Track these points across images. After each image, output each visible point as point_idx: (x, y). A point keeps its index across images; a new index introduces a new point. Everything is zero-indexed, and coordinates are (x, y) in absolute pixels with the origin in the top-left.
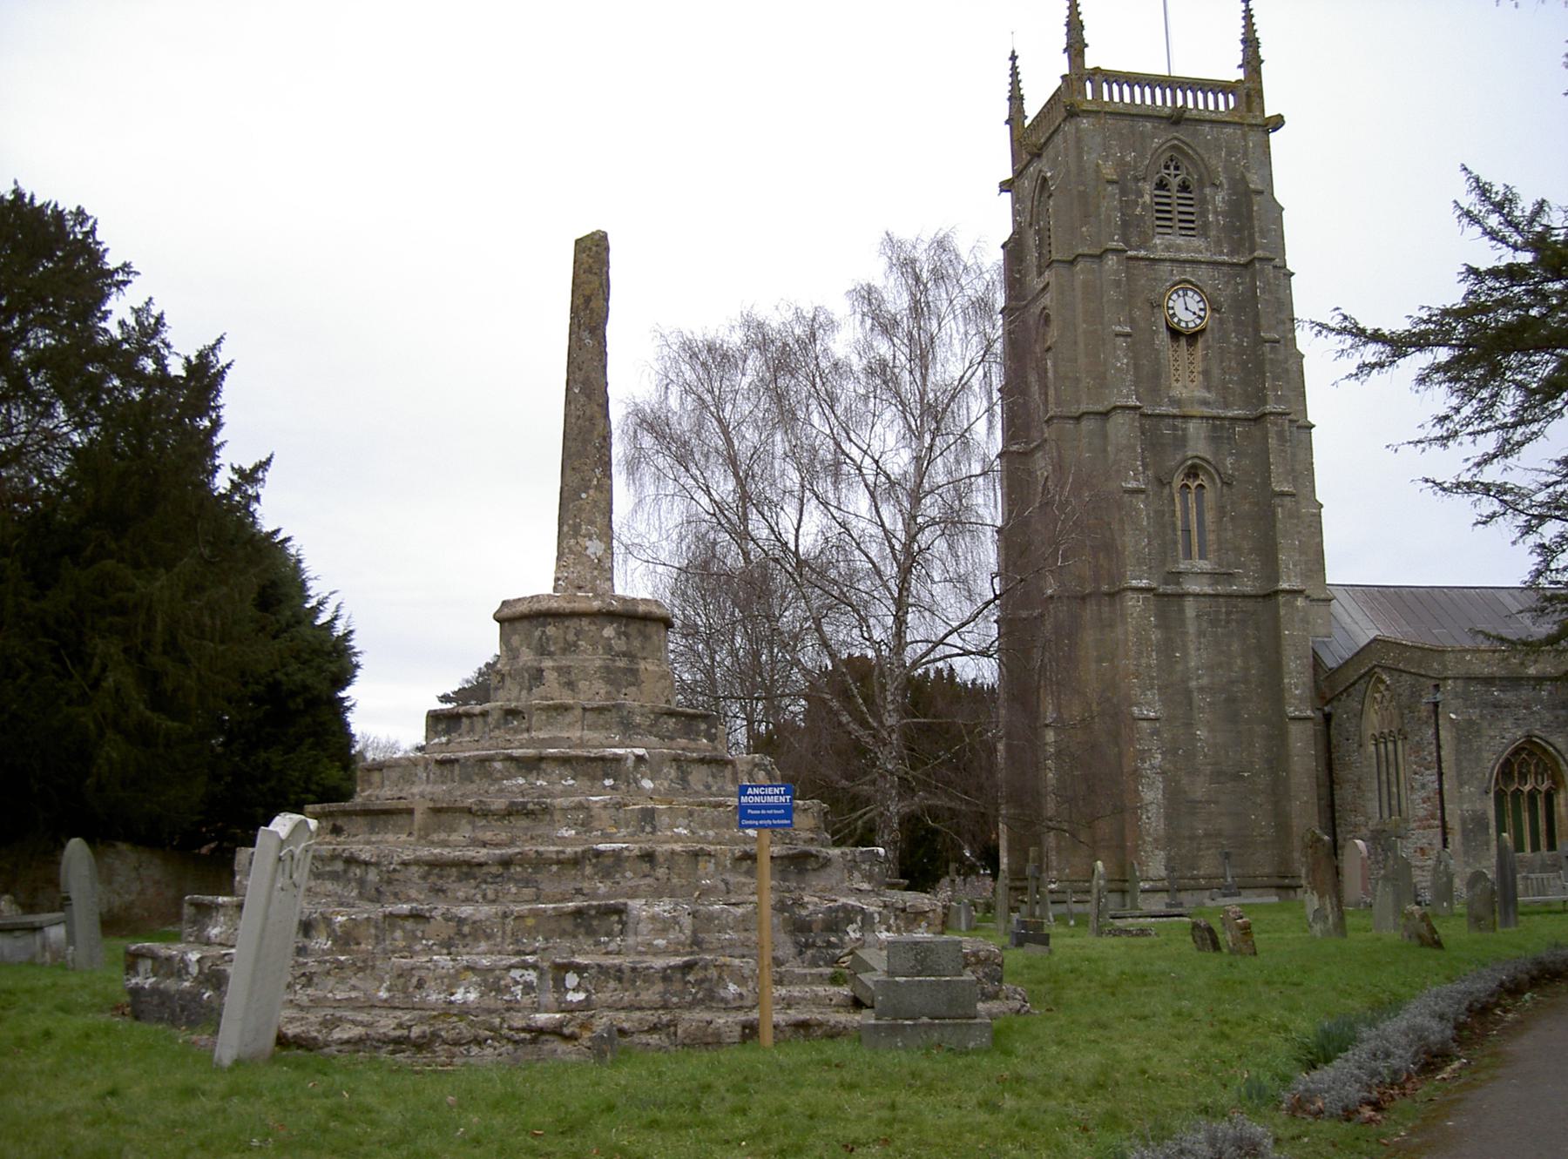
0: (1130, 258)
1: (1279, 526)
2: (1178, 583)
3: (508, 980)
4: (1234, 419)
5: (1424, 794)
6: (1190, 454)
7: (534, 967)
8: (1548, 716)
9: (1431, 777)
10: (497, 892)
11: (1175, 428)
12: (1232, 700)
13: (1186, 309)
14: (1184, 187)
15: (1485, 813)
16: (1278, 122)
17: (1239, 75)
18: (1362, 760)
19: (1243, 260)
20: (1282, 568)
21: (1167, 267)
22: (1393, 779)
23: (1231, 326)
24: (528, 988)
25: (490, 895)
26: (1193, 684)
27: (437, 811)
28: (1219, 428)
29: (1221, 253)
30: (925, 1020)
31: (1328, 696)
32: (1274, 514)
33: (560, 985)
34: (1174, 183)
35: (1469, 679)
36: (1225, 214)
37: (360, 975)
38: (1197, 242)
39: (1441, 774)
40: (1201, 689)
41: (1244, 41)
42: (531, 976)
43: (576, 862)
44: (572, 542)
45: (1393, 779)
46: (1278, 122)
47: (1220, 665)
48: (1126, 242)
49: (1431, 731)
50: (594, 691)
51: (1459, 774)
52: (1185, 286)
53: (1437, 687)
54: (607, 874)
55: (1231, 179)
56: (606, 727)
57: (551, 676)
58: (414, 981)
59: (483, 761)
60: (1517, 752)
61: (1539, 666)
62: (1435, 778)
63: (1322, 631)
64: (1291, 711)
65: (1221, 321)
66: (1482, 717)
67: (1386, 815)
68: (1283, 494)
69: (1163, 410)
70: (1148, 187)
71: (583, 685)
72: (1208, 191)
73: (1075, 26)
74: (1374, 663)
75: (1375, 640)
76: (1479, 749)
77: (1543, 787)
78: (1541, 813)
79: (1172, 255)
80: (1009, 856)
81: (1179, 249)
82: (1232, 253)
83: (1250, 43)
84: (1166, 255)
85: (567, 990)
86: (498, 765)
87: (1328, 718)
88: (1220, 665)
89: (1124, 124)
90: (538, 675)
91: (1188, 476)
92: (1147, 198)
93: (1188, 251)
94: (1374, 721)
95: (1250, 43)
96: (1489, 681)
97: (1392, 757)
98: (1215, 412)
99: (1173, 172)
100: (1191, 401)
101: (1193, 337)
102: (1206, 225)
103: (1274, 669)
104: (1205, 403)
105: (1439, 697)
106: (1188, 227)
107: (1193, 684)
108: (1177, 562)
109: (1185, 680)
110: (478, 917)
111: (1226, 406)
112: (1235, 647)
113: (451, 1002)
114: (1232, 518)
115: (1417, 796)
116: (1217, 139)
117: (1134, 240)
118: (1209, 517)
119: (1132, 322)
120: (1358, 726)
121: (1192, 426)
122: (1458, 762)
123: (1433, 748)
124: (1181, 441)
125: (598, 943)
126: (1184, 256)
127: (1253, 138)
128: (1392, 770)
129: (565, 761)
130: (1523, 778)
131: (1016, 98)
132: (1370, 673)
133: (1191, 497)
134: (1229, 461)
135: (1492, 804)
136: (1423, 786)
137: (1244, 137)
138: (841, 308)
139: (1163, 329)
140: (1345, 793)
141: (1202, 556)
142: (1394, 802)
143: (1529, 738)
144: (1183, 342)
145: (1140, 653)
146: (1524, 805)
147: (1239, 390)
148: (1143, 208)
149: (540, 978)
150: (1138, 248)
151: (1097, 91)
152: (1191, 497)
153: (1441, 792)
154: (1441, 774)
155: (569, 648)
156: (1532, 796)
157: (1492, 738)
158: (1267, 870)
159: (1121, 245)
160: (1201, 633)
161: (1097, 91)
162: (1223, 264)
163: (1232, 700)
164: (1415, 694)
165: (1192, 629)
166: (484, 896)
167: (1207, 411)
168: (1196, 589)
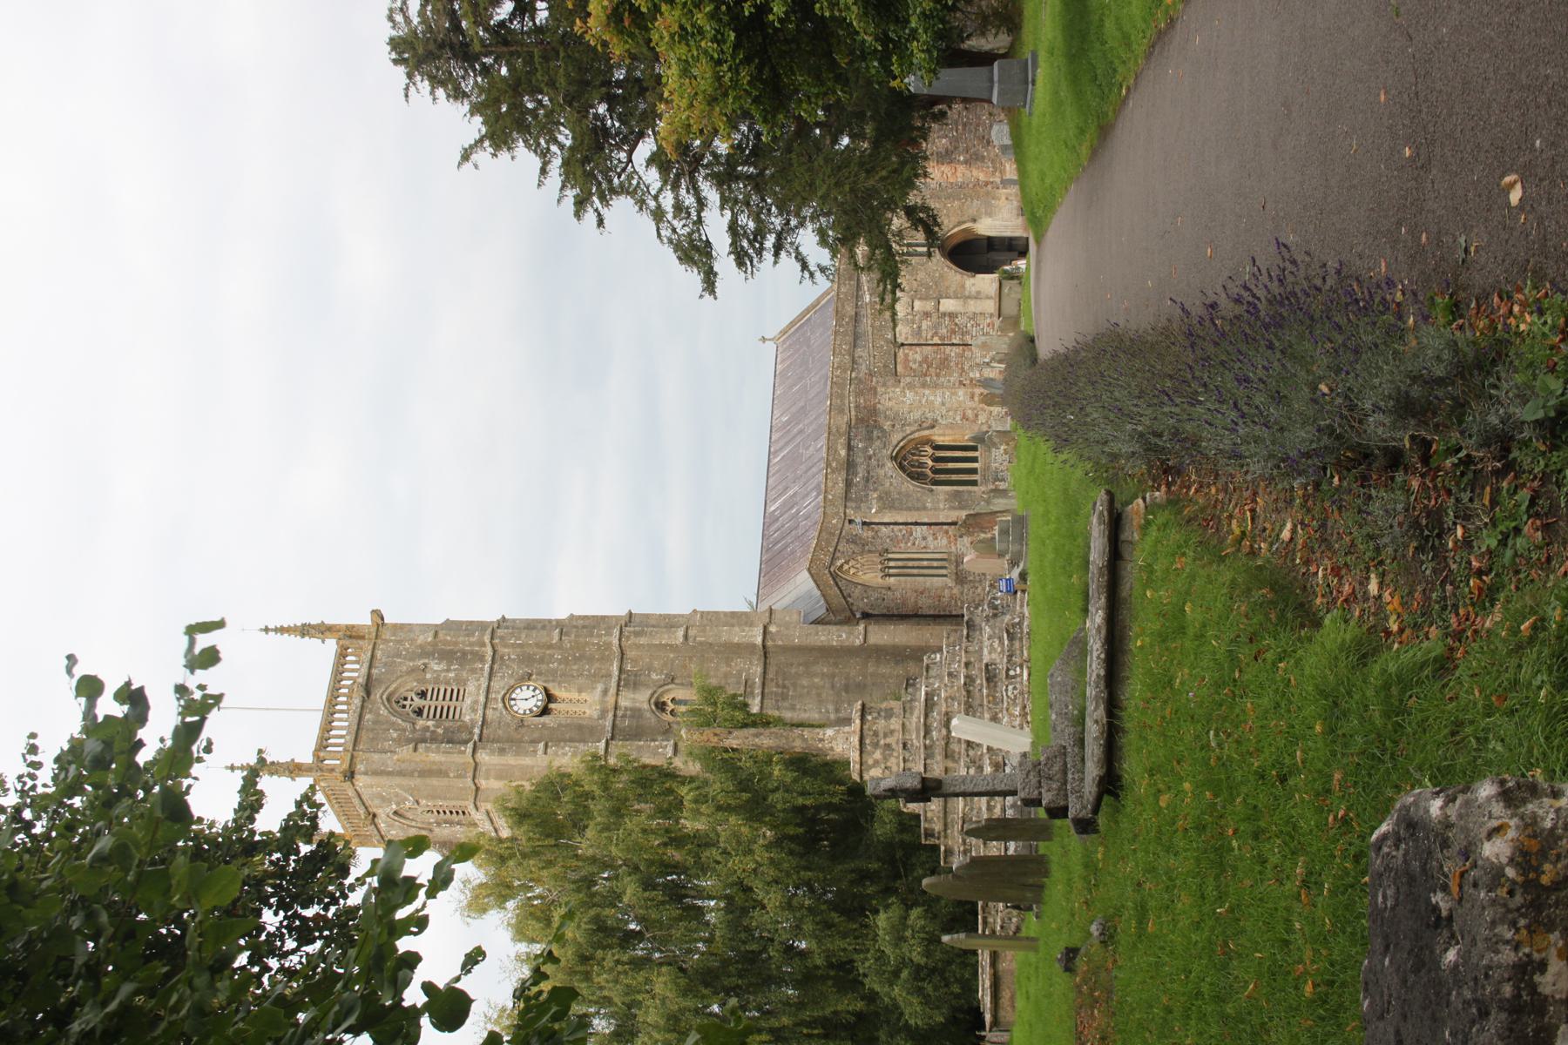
4: (621, 670)
5: (930, 538)
6: (646, 706)
8: (878, 443)
9: (919, 531)
11: (624, 716)
12: (847, 688)
14: (423, 695)
16: (377, 614)
18: (902, 588)
21: (489, 713)
22: (916, 564)
23: (544, 667)
27: (946, 756)
28: (628, 681)
31: (848, 614)
32: (701, 643)
33: (1014, 677)
34: (418, 702)
35: (846, 498)
36: (450, 663)
38: (471, 688)
39: (916, 524)
40: (837, 711)
41: (303, 635)
43: (968, 692)
45: (916, 564)
46: (377, 614)
47: (819, 695)
48: (466, 742)
49: (883, 529)
50: (895, 724)
51: (918, 509)
52: (507, 699)
53: (851, 522)
54: (973, 681)
57: (888, 740)
59: (926, 747)
60: (902, 467)
62: (919, 528)
63: (795, 617)
65: (539, 674)
66: (875, 490)
67: (944, 572)
68: (686, 637)
70: (421, 723)
72: (428, 676)
74: (829, 576)
77: (930, 451)
79: (481, 708)
83: (305, 630)
84: (480, 712)
87: (866, 616)
88: (819, 695)
89: (364, 735)
90: (888, 746)
91: (663, 710)
92: (430, 723)
94: (872, 577)
95: (305, 630)
96: (849, 484)
97: (900, 564)
99: (407, 703)
100: (602, 702)
101: (550, 698)
103: (826, 652)
104: (605, 692)
105: (858, 520)
111: (609, 676)
112: (805, 682)
115: (932, 543)
117: (464, 736)
119: (534, 742)
120: (874, 589)
121: (623, 703)
122: (909, 509)
123: (896, 528)
124: (636, 713)
126: (482, 699)
127: (386, 635)
128: (910, 564)
129: (926, 716)
130: (922, 465)
132: (834, 576)
134: (654, 676)
135: (940, 488)
136: (924, 538)
137: (386, 641)
139: (542, 719)
140: (925, 604)
142: (935, 564)
143: (894, 458)
144: (552, 706)
147: (597, 665)
150: (471, 733)
151: (334, 755)
153: (930, 524)
154: (916, 524)
155: (876, 734)
159: (470, 745)
161: (334, 755)
162: (491, 668)
163: (847, 688)
164: (854, 540)
167: (613, 690)
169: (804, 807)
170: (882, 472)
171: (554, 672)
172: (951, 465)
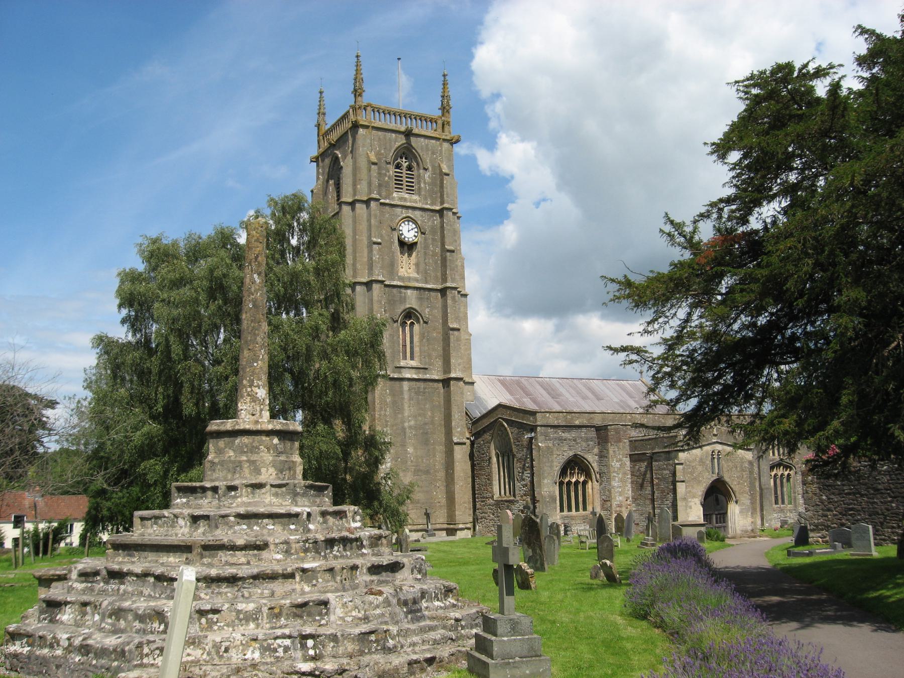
0: (382, 204)
1: (451, 345)
2: (400, 373)
3: (275, 645)
7: (290, 637)
10: (250, 593)
13: (409, 232)
15: (554, 492)
17: (440, 113)
19: (438, 208)
20: (452, 367)
23: (430, 241)
24: (286, 649)
25: (246, 595)
26: (406, 424)
29: (427, 204)
30: (517, 659)
33: (304, 647)
37: (192, 647)
40: (410, 427)
42: (287, 642)
44: (249, 389)
47: (420, 415)
54: (308, 581)
55: (433, 167)
56: (283, 496)
58: (223, 649)
61: (580, 420)
64: (455, 440)
65: (425, 239)
69: (395, 283)
71: (263, 470)
72: (422, 171)
73: (358, 79)
75: (500, 406)
76: (552, 461)
77: (582, 479)
78: (580, 492)
81: (405, 200)
82: (432, 204)
84: (399, 203)
85: (308, 649)
86: (232, 519)
93: (410, 202)
98: (420, 285)
100: (409, 279)
102: (420, 188)
104: (417, 280)
106: (410, 190)
107: (406, 424)
108: (399, 361)
109: (403, 422)
110: (247, 609)
111: (426, 283)
113: (245, 660)
114: (428, 340)
116: (427, 145)
117: (384, 194)
118: (416, 339)
125: (315, 620)
126: (408, 204)
130: (572, 474)
131: (321, 113)
133: (407, 328)
134: (427, 310)
137: (441, 145)
139: (396, 241)
141: (412, 358)
144: (406, 248)
145: (381, 408)
146: (572, 488)
148: (389, 177)
149: (293, 643)
152: (407, 328)
156: (577, 483)
157: (558, 455)
158: (441, 520)
159: (378, 197)
160: (411, 399)
165: (406, 396)
166: (243, 596)
168: (408, 376)
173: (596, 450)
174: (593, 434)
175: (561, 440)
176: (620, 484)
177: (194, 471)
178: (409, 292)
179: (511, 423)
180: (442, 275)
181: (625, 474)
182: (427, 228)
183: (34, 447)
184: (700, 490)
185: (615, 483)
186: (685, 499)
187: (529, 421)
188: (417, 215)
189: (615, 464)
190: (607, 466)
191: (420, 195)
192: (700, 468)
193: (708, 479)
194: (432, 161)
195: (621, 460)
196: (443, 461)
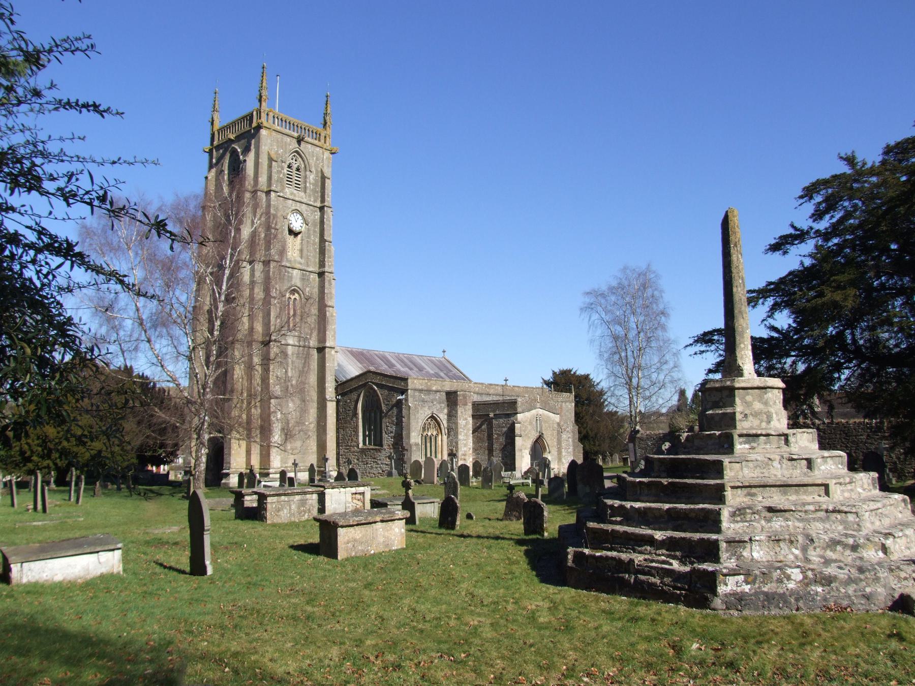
14: (298, 170)
34: (295, 166)
55: (317, 171)
64: (327, 397)
65: (308, 230)
72: (308, 173)
77: (435, 433)
78: (433, 443)
80: (714, 485)
84: (291, 197)
96: (421, 391)
98: (304, 268)
102: (305, 187)
104: (301, 264)
126: (297, 199)
138: (680, 376)
146: (428, 440)
169: (12, 397)
170: (426, 409)
171: (309, 237)
172: (428, 445)
173: (446, 411)
174: (805, 462)
175: (423, 401)
176: (465, 438)
177: (142, 365)
178: (295, 272)
179: (380, 386)
180: (320, 261)
181: (468, 430)
182: (310, 220)
183: (67, 363)
184: (529, 444)
185: (461, 437)
186: (521, 450)
187: (401, 385)
188: (303, 208)
189: (461, 422)
190: (456, 424)
191: (305, 192)
192: (529, 427)
193: (534, 436)
194: (316, 166)
195: (466, 419)
196: (315, 416)
